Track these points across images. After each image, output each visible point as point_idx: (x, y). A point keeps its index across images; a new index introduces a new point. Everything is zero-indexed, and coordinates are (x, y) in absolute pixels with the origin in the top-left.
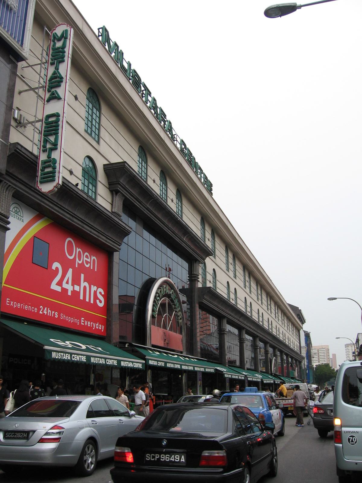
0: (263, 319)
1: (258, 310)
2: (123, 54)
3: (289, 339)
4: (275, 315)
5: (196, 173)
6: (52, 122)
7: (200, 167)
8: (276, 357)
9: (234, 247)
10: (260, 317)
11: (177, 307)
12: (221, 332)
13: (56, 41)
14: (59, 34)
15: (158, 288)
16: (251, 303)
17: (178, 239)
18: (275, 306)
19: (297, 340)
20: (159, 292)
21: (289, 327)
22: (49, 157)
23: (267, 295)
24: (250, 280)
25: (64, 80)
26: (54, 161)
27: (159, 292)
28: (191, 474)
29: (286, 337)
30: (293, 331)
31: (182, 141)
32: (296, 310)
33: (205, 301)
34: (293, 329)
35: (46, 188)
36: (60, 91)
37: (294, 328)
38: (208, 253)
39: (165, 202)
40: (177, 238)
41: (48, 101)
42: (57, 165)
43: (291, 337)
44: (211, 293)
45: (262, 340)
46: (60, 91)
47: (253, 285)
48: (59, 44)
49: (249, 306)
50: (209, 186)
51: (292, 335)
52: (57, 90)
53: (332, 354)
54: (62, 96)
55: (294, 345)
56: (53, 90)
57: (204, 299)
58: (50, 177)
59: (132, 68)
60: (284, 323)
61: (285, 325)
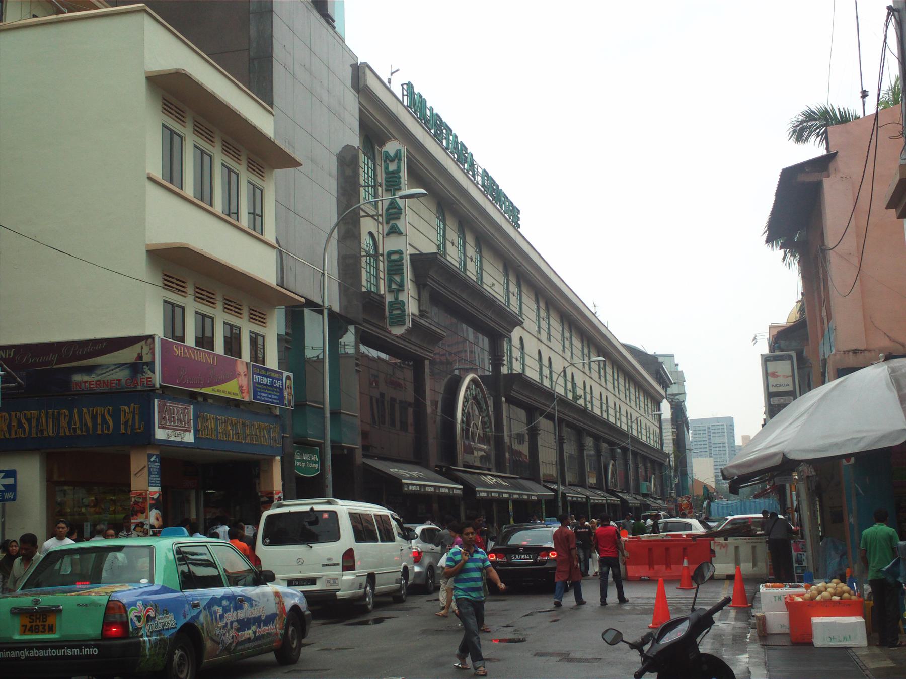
0: (592, 398)
1: (539, 352)
2: (426, 101)
3: (618, 410)
4: (613, 384)
5: (437, 137)
6: (396, 260)
7: (504, 194)
8: (615, 461)
9: (557, 302)
10: (587, 394)
11: (483, 410)
12: (533, 433)
13: (388, 162)
14: (392, 154)
15: (466, 391)
16: (550, 358)
17: (482, 316)
18: (635, 387)
19: (654, 423)
20: (466, 396)
21: (605, 372)
22: (396, 298)
23: (634, 385)
24: (520, 291)
25: (403, 211)
26: (403, 303)
27: (466, 396)
28: (383, 588)
29: (642, 426)
30: (646, 407)
31: (485, 171)
32: (653, 363)
33: (513, 394)
34: (646, 403)
35: (398, 331)
36: (400, 224)
37: (649, 401)
38: (515, 322)
39: (461, 271)
40: (480, 315)
41: (388, 234)
42: (406, 307)
43: (651, 424)
44: (520, 379)
45: (591, 434)
46: (400, 224)
47: (555, 324)
48: (392, 167)
49: (519, 346)
50: (513, 213)
51: (612, 391)
52: (397, 224)
53: (742, 436)
54: (403, 230)
55: (648, 433)
56: (392, 222)
57: (514, 391)
58: (399, 320)
59: (434, 112)
60: (639, 403)
61: (607, 378)
